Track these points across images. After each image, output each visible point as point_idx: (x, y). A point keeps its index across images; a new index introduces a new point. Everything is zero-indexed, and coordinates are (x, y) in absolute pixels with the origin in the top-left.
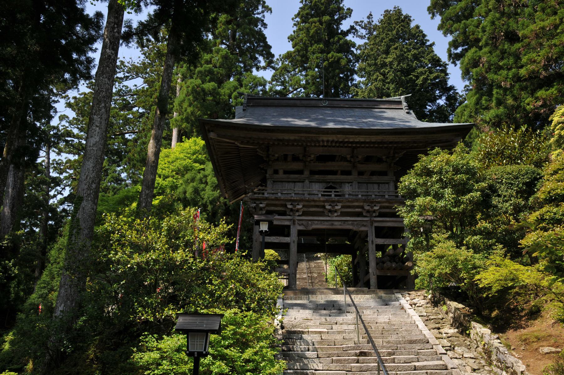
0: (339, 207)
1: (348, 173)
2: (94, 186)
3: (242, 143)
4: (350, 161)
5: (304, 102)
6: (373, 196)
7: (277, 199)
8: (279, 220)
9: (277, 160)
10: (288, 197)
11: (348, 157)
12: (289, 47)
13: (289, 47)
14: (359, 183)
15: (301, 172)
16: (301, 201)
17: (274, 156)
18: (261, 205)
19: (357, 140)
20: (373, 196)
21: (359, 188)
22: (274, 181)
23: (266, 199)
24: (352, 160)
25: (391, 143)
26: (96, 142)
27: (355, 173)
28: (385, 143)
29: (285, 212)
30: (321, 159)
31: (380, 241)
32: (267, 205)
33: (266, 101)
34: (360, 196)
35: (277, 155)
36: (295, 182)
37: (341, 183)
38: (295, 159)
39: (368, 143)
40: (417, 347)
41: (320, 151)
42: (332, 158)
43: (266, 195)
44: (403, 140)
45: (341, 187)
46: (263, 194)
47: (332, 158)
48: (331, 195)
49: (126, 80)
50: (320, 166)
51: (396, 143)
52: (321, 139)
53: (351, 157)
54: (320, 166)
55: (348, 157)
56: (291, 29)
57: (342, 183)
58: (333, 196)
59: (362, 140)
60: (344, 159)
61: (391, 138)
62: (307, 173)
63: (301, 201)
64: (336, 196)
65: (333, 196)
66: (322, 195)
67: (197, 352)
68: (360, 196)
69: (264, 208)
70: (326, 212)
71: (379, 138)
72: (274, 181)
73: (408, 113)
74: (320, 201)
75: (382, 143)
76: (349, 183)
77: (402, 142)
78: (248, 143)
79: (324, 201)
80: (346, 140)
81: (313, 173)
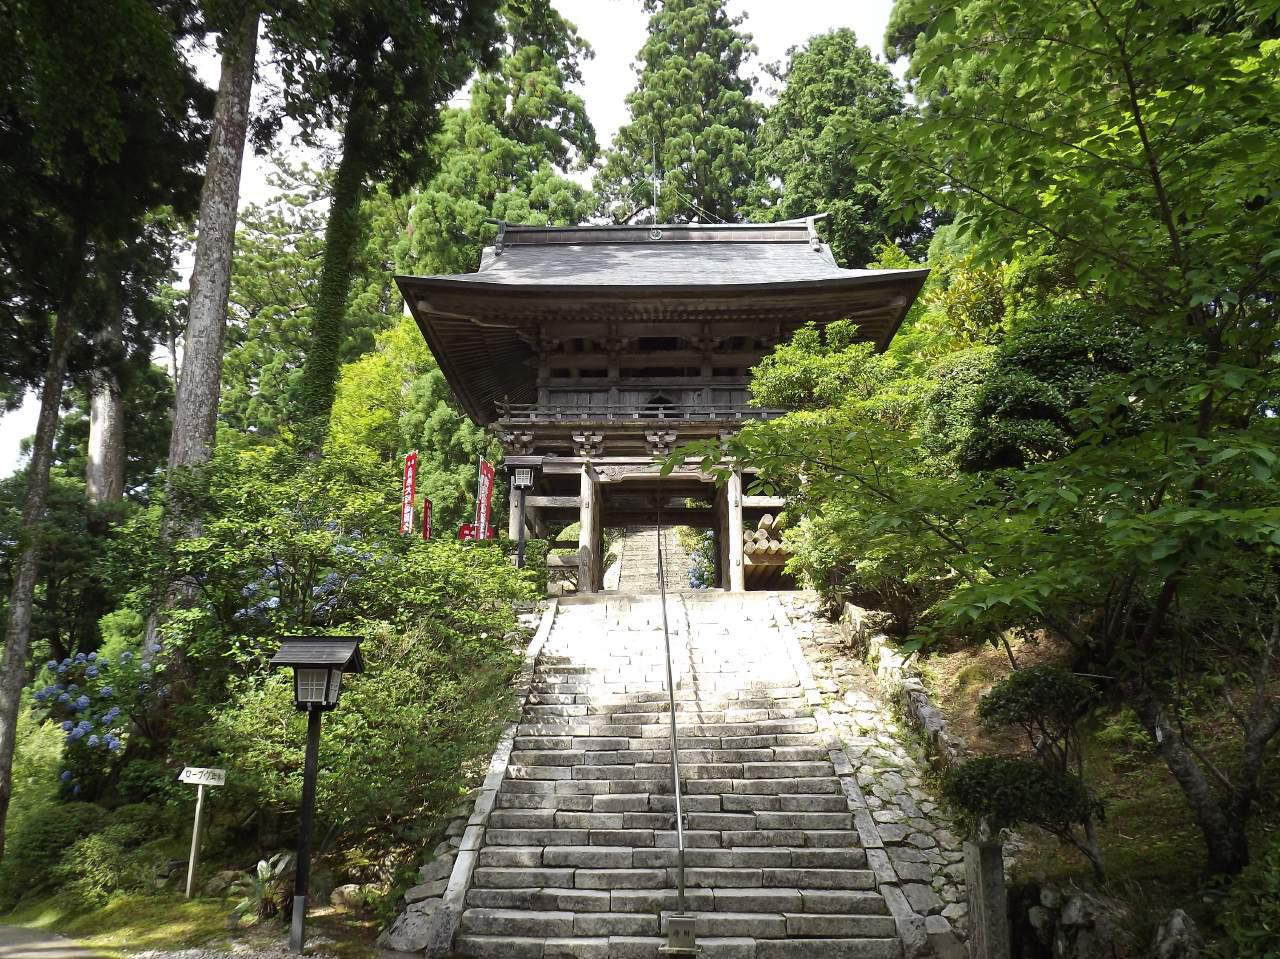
0: (673, 438)
1: (696, 372)
2: (205, 410)
3: (485, 319)
4: (698, 349)
5: (615, 235)
6: (739, 416)
7: (552, 426)
8: (553, 465)
9: (560, 348)
10: (576, 422)
11: (695, 340)
12: (626, 119)
13: (626, 119)
14: (714, 390)
15: (603, 373)
16: (600, 428)
17: (549, 342)
18: (525, 438)
19: (701, 307)
20: (739, 416)
21: (714, 401)
22: (551, 392)
23: (533, 426)
24: (702, 346)
25: (768, 311)
26: (206, 328)
27: (706, 372)
28: (756, 312)
29: (572, 449)
30: (647, 345)
31: (753, 501)
32: (536, 438)
33: (621, 235)
34: (712, 416)
35: (556, 341)
36: (591, 392)
37: (680, 392)
38: (596, 347)
39: (722, 312)
40: (420, 904)
41: (639, 331)
42: (670, 344)
43: (533, 418)
44: (791, 304)
45: (680, 399)
46: (528, 416)
47: (670, 344)
48: (656, 416)
49: (314, 199)
50: (641, 360)
51: (779, 310)
52: (631, 308)
53: (701, 341)
54: (641, 360)
55: (695, 340)
56: (631, 81)
57: (682, 390)
58: (661, 416)
59: (712, 307)
60: (687, 345)
61: (770, 302)
62: (613, 374)
63: (600, 428)
64: (666, 416)
65: (661, 416)
66: (641, 416)
67: (205, 786)
68: (712, 416)
69: (530, 442)
70: (647, 447)
71: (745, 302)
72: (551, 392)
73: (817, 250)
74: (634, 428)
75: (749, 311)
76: (695, 390)
77: (790, 310)
78: (496, 319)
79: (645, 428)
80: (681, 308)
81: (625, 373)
